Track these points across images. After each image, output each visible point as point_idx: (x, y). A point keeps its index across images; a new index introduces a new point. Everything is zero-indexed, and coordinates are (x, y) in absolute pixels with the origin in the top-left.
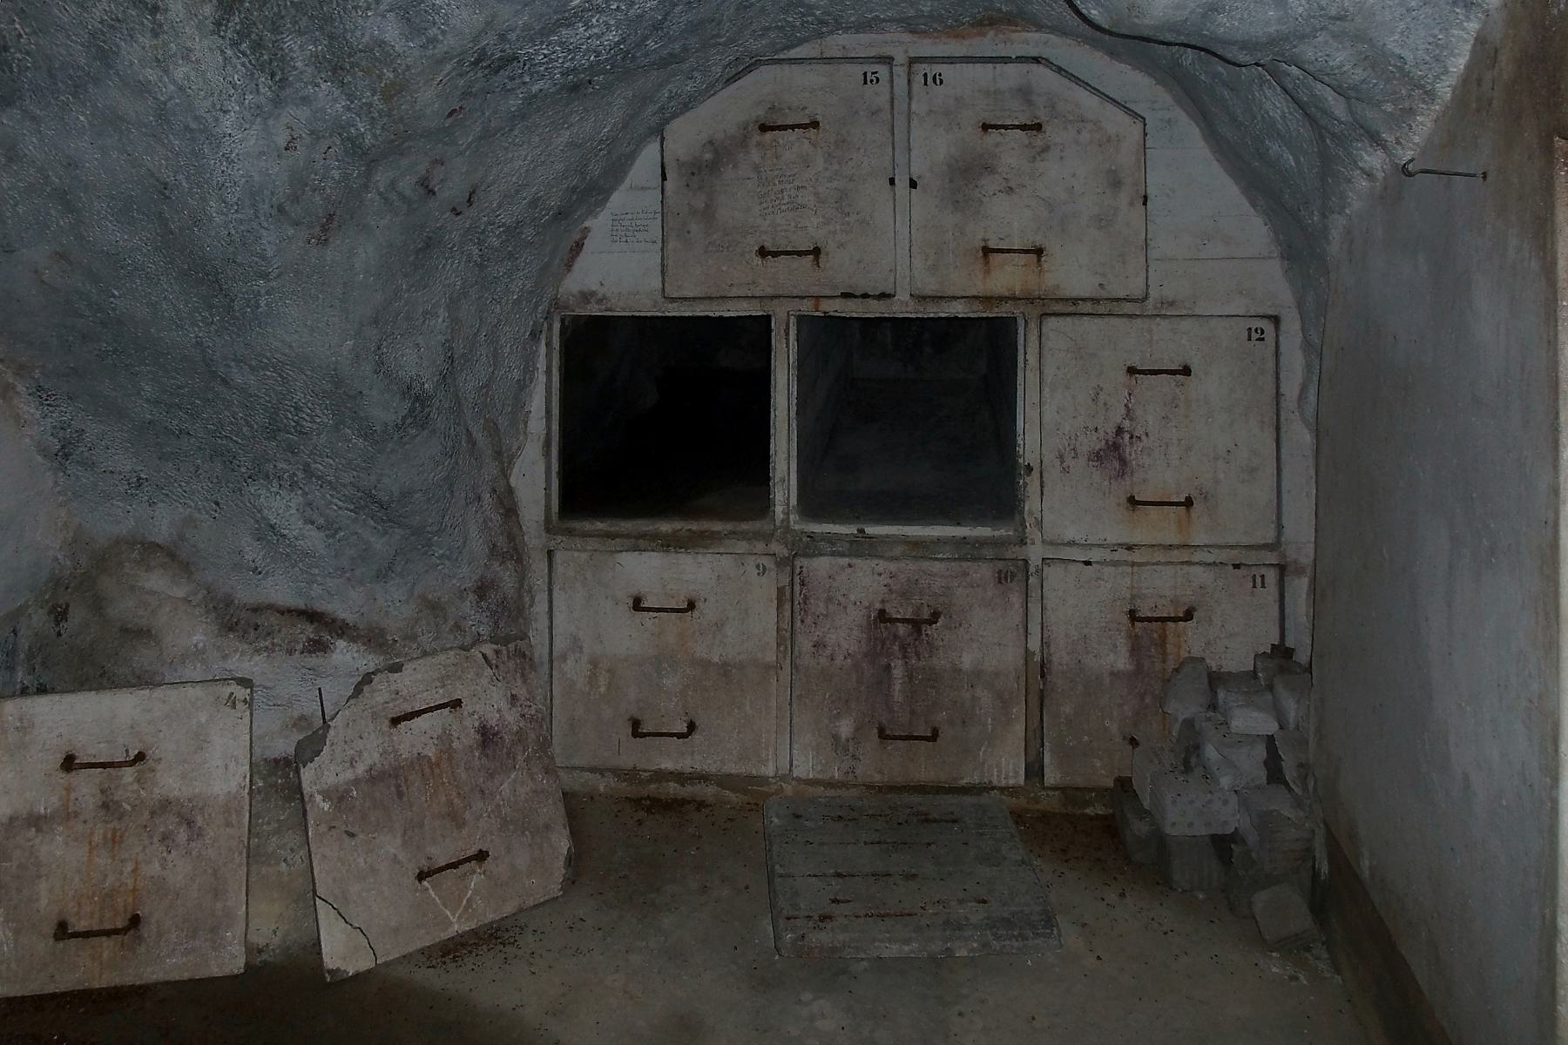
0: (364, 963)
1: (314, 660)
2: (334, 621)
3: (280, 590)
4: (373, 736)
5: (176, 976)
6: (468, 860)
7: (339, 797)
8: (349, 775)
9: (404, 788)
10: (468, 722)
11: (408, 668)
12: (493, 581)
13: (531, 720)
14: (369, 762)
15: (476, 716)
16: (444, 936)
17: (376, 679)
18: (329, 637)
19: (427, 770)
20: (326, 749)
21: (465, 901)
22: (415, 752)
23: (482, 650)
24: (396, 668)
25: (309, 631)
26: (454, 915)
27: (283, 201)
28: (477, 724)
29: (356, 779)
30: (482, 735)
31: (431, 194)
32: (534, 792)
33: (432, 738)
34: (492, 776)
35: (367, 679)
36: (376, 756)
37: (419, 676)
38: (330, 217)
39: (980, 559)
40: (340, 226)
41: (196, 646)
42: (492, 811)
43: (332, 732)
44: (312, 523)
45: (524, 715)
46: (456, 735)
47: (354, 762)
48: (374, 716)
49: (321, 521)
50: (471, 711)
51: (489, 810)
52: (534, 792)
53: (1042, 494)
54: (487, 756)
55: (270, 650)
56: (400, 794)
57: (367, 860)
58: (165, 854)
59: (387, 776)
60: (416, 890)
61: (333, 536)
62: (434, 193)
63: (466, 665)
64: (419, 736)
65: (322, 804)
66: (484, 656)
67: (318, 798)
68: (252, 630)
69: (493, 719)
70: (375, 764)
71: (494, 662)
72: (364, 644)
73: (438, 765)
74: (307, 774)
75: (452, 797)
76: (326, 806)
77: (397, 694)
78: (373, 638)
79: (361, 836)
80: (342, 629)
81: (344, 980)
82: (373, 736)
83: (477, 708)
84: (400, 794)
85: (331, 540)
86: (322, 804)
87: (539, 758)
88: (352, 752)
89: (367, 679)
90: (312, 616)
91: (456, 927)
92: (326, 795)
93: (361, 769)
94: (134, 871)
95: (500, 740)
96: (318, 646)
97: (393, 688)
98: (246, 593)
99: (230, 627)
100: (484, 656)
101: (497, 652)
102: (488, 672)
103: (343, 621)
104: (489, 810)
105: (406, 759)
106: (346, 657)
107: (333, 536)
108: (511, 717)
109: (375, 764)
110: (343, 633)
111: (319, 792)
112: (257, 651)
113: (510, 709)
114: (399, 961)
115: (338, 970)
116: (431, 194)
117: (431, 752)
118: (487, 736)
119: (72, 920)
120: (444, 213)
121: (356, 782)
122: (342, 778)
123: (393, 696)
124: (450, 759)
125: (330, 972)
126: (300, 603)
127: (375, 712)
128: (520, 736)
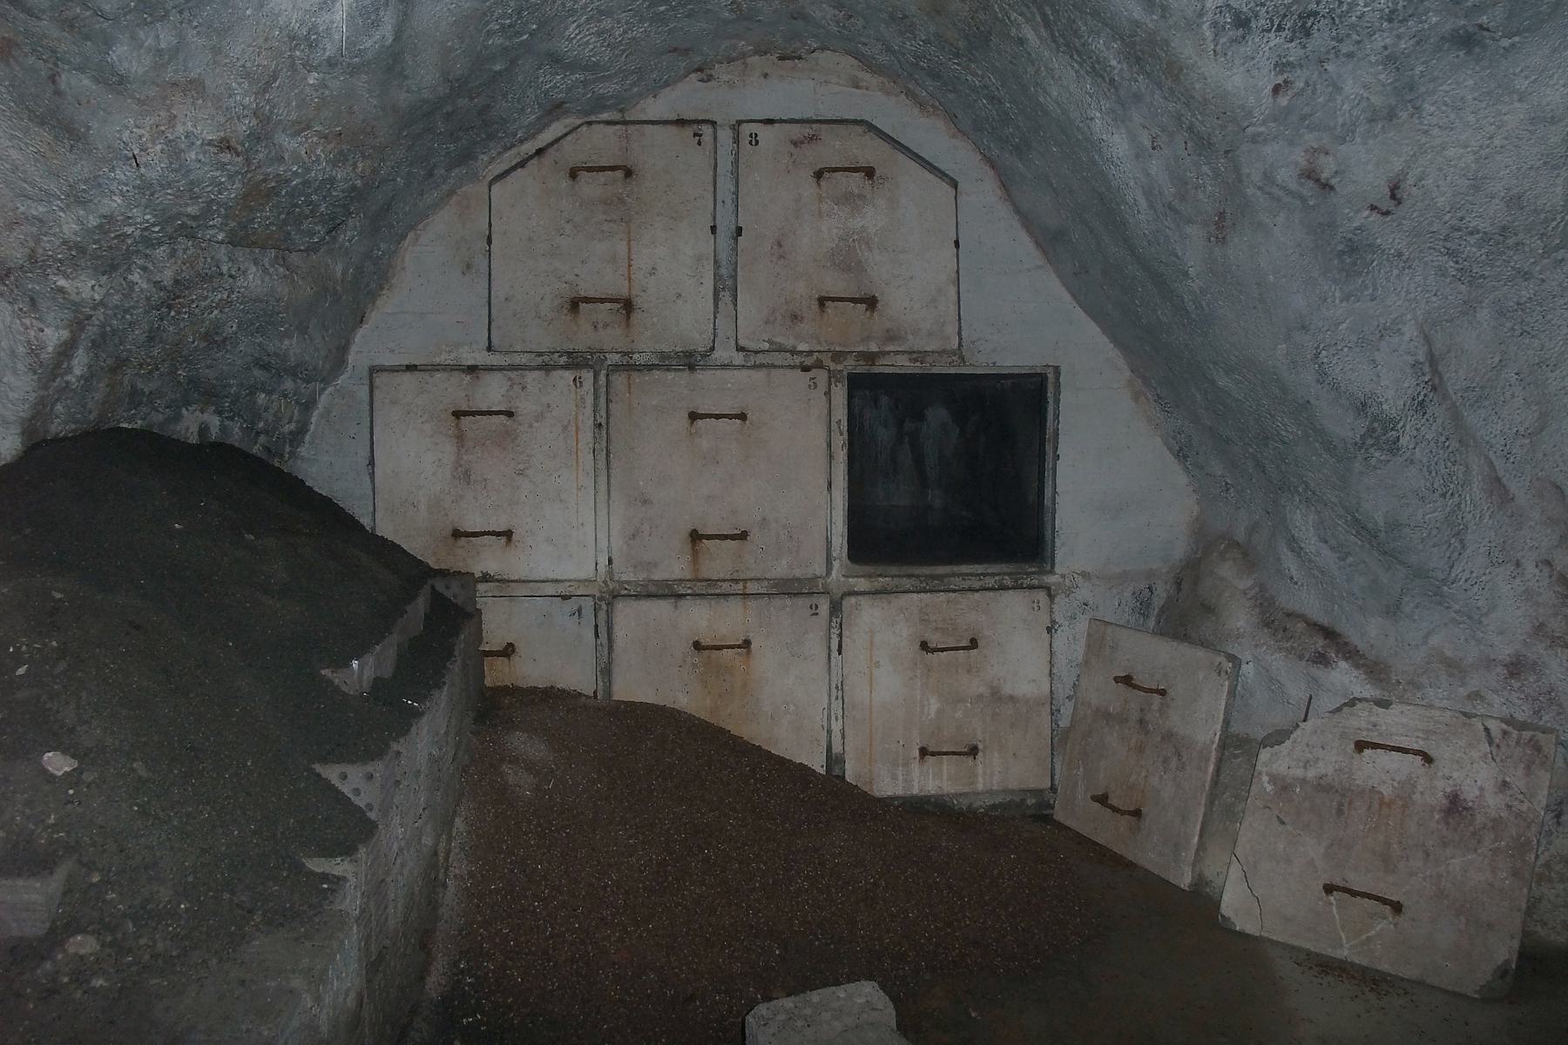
0: (1251, 928)
1: (1318, 671)
2: (1346, 644)
3: (1310, 603)
4: (1334, 751)
5: (1149, 867)
6: (1384, 901)
7: (1284, 787)
8: (1299, 772)
9: (1345, 808)
10: (1440, 784)
11: (1396, 709)
12: (1535, 663)
13: (1518, 815)
14: (1323, 772)
15: (1451, 782)
16: (1329, 952)
17: (1359, 705)
18: (1333, 655)
19: (1376, 806)
20: (1288, 743)
21: (1364, 937)
22: (1370, 783)
23: (1485, 723)
24: (1384, 704)
25: (1320, 643)
26: (1347, 943)
27: (1171, 199)
28: (1449, 790)
29: (1304, 780)
30: (1451, 802)
31: (1327, 189)
32: (1490, 884)
33: (1393, 780)
34: (1445, 845)
35: (1352, 703)
36: (1330, 771)
37: (1405, 720)
38: (1222, 215)
39: (1042, 384)
40: (1234, 224)
41: (1238, 629)
42: (1431, 876)
43: (1298, 732)
44: (1326, 542)
45: (1511, 807)
46: (1420, 788)
47: (1308, 765)
48: (1343, 735)
49: (1333, 542)
50: (1447, 775)
51: (1428, 873)
52: (1490, 884)
53: (958, 272)
54: (1447, 824)
55: (1289, 651)
56: (1340, 812)
57: (1287, 849)
58: (1162, 773)
59: (1334, 790)
60: (1321, 899)
61: (1344, 559)
62: (1332, 188)
63: (1460, 731)
64: (1379, 770)
65: (1266, 785)
66: (1487, 730)
67: (1265, 778)
68: (1281, 631)
69: (1470, 794)
70: (1326, 775)
71: (1497, 740)
72: (1366, 673)
73: (1389, 805)
74: (1265, 755)
75: (1392, 841)
76: (1269, 788)
77: (1375, 726)
78: (1375, 670)
79: (1289, 827)
80: (1351, 654)
81: (1230, 929)
82: (1334, 751)
83: (1455, 775)
84: (1340, 812)
85: (1342, 563)
86: (1266, 785)
87: (1513, 856)
88: (1310, 755)
89: (1352, 703)
90: (1329, 634)
91: (1346, 953)
92: (1274, 779)
93: (1311, 774)
94: (1146, 777)
95: (1469, 817)
96: (1321, 660)
97: (1373, 719)
98: (1288, 600)
99: (1267, 624)
100: (1487, 730)
101: (1505, 733)
102: (1485, 747)
103: (1356, 646)
104: (1428, 873)
105: (1358, 785)
106: (1343, 677)
107: (1344, 559)
108: (1494, 802)
109: (1326, 775)
110: (1350, 657)
111: (1268, 774)
112: (1280, 649)
113: (1496, 793)
114: (1284, 946)
115: (1229, 918)
116: (1327, 189)
117: (1387, 791)
118: (1455, 806)
119: (1111, 796)
120: (1358, 211)
121: (1303, 781)
122: (1292, 772)
123: (1370, 727)
124: (1405, 807)
125: (1223, 916)
126: (1324, 620)
127: (1346, 733)
128: (1497, 824)
